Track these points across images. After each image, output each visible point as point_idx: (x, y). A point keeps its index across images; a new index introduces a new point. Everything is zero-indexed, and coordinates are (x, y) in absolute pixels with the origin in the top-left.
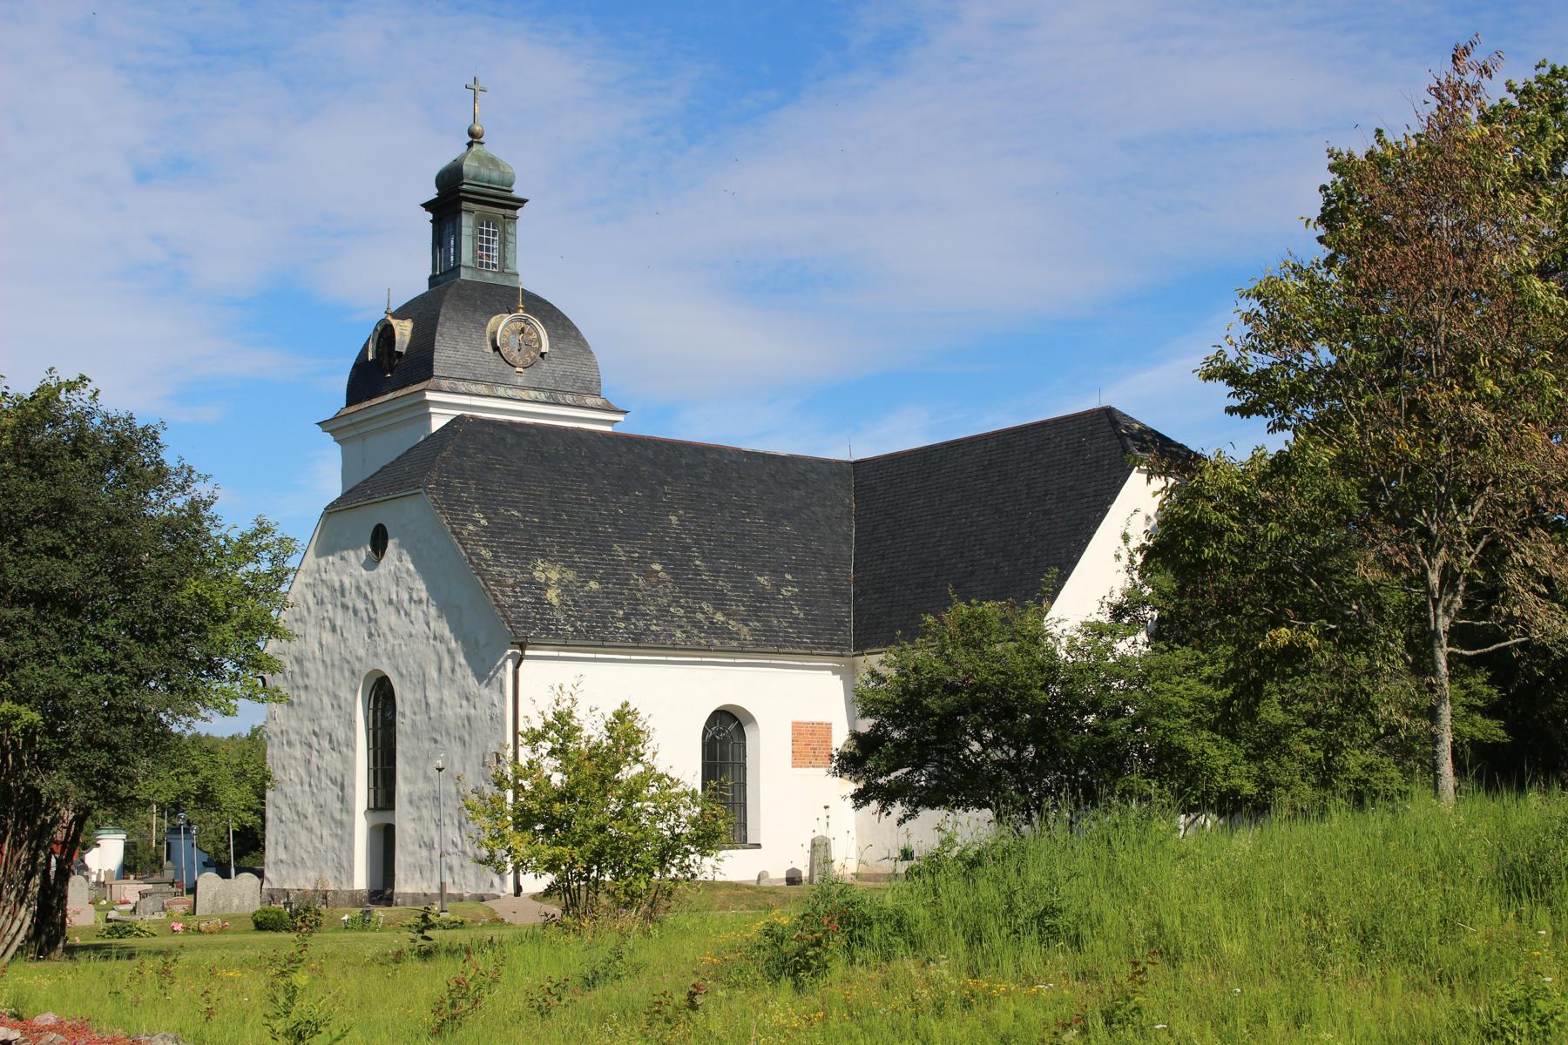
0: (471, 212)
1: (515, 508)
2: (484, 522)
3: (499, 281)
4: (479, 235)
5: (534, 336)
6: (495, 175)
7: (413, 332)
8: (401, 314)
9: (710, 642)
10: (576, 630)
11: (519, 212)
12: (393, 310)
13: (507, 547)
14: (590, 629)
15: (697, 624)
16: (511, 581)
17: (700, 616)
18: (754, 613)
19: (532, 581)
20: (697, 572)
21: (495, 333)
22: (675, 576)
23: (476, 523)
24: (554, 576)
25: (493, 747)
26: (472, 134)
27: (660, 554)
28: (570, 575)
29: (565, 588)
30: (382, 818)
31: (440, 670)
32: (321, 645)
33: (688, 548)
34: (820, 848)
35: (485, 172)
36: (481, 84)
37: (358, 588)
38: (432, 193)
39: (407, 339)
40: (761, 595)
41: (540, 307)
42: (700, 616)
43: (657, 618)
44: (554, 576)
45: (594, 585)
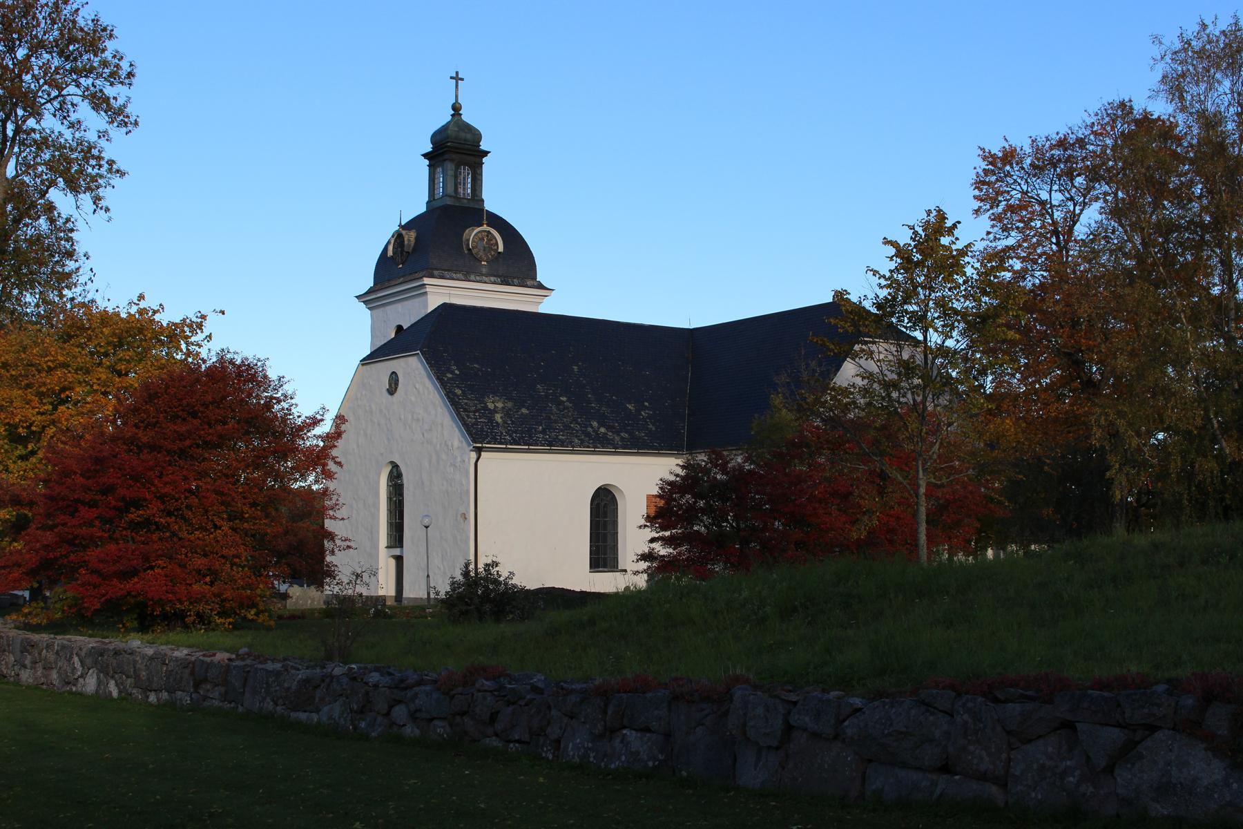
0: (452, 160)
3: (472, 205)
6: (469, 136)
7: (417, 239)
15: (588, 435)
17: (590, 429)
19: (486, 408)
23: (452, 372)
24: (500, 405)
28: (510, 405)
29: (507, 413)
30: (397, 552)
31: (430, 462)
35: (462, 135)
37: (381, 411)
38: (428, 148)
39: (413, 243)
42: (590, 429)
44: (500, 405)
45: (524, 411)
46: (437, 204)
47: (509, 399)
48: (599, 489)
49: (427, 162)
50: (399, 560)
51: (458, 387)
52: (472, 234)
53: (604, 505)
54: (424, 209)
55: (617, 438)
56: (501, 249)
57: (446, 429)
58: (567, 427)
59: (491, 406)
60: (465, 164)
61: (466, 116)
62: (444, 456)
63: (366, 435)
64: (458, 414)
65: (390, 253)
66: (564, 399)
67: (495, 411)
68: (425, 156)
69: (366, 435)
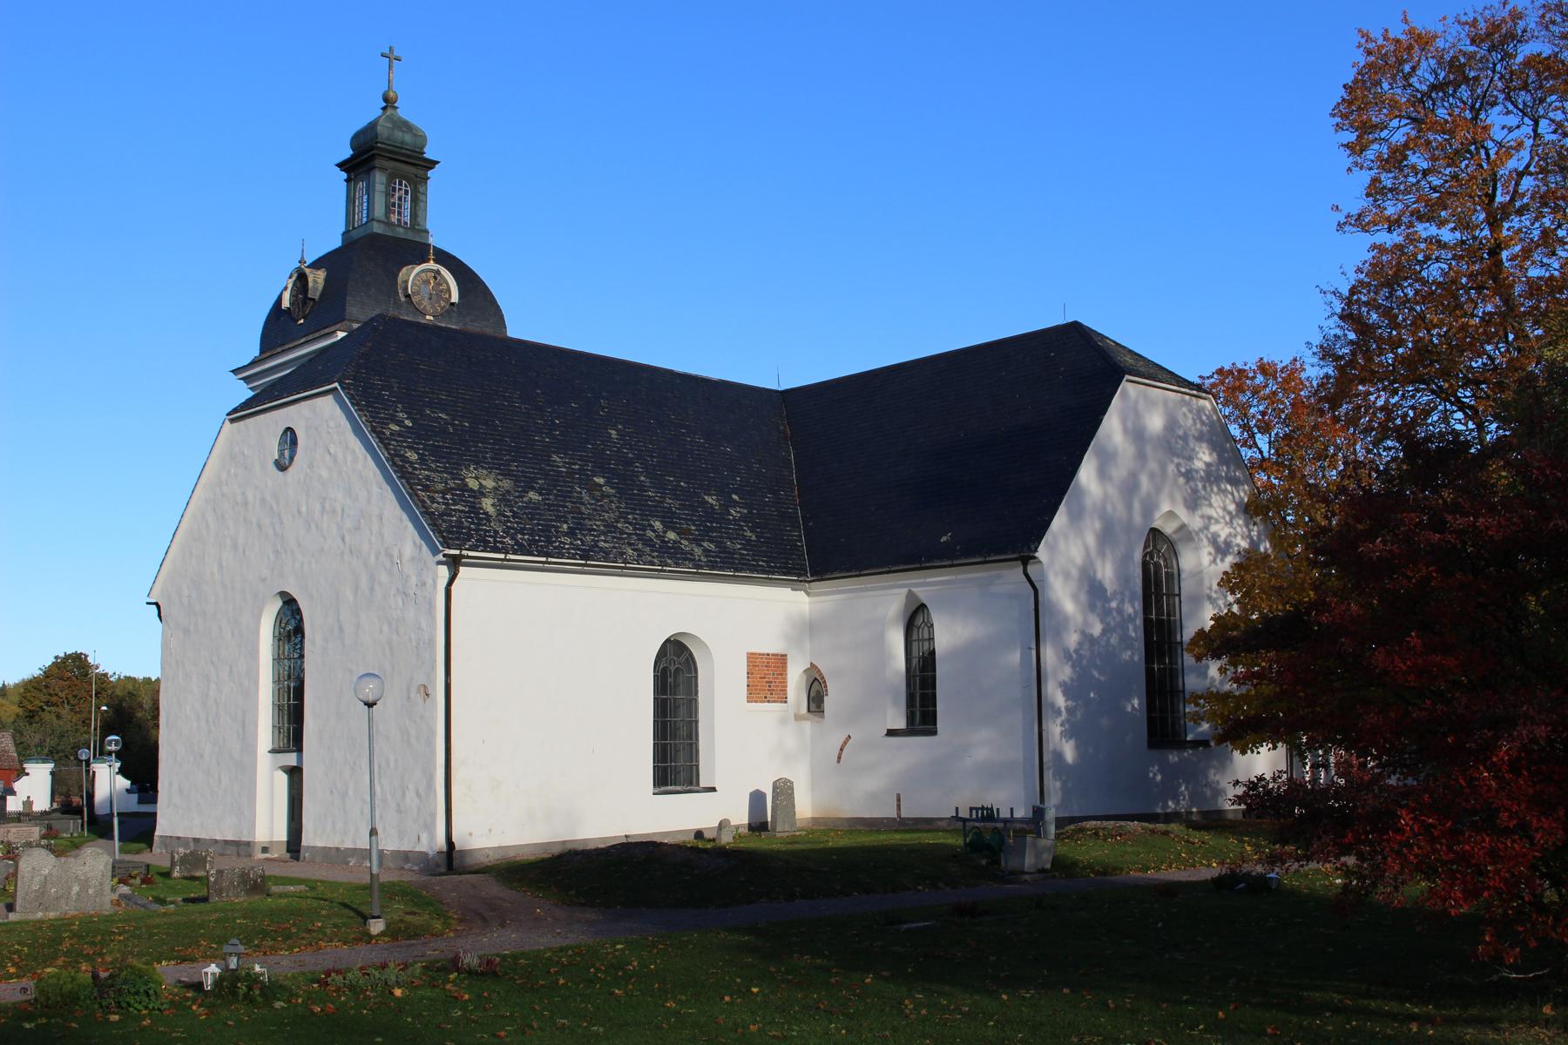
0: (383, 169)
1: (443, 410)
2: (408, 423)
3: (410, 236)
4: (389, 194)
5: (444, 287)
6: (408, 138)
7: (326, 280)
8: (316, 265)
9: (665, 558)
10: (517, 543)
11: (430, 173)
12: (309, 260)
13: (436, 452)
14: (532, 542)
15: (648, 542)
16: (441, 487)
17: (650, 534)
18: (705, 534)
19: (464, 487)
20: (642, 488)
21: (406, 282)
22: (620, 491)
23: (400, 423)
24: (489, 484)
25: (420, 679)
26: (386, 99)
27: (602, 468)
28: (507, 484)
29: (503, 499)
30: (291, 759)
31: (356, 589)
32: (221, 566)
33: (629, 463)
34: (783, 790)
35: (398, 135)
36: (396, 53)
37: (263, 501)
38: (347, 153)
39: (321, 287)
40: (710, 512)
41: (445, 258)
42: (650, 534)
43: (605, 534)
44: (489, 484)
45: (533, 495)
46: (356, 234)
47: (507, 474)
48: (668, 641)
49: (344, 175)
50: (295, 774)
51: (411, 448)
52: (412, 275)
53: (675, 670)
54: (336, 243)
55: (698, 551)
56: (455, 298)
57: (393, 530)
58: (610, 528)
59: (473, 484)
60: (402, 177)
61: (404, 111)
62: (384, 577)
63: (235, 546)
64: (413, 494)
65: (286, 304)
66: (601, 481)
67: (481, 493)
68: (341, 165)
69: (235, 546)
